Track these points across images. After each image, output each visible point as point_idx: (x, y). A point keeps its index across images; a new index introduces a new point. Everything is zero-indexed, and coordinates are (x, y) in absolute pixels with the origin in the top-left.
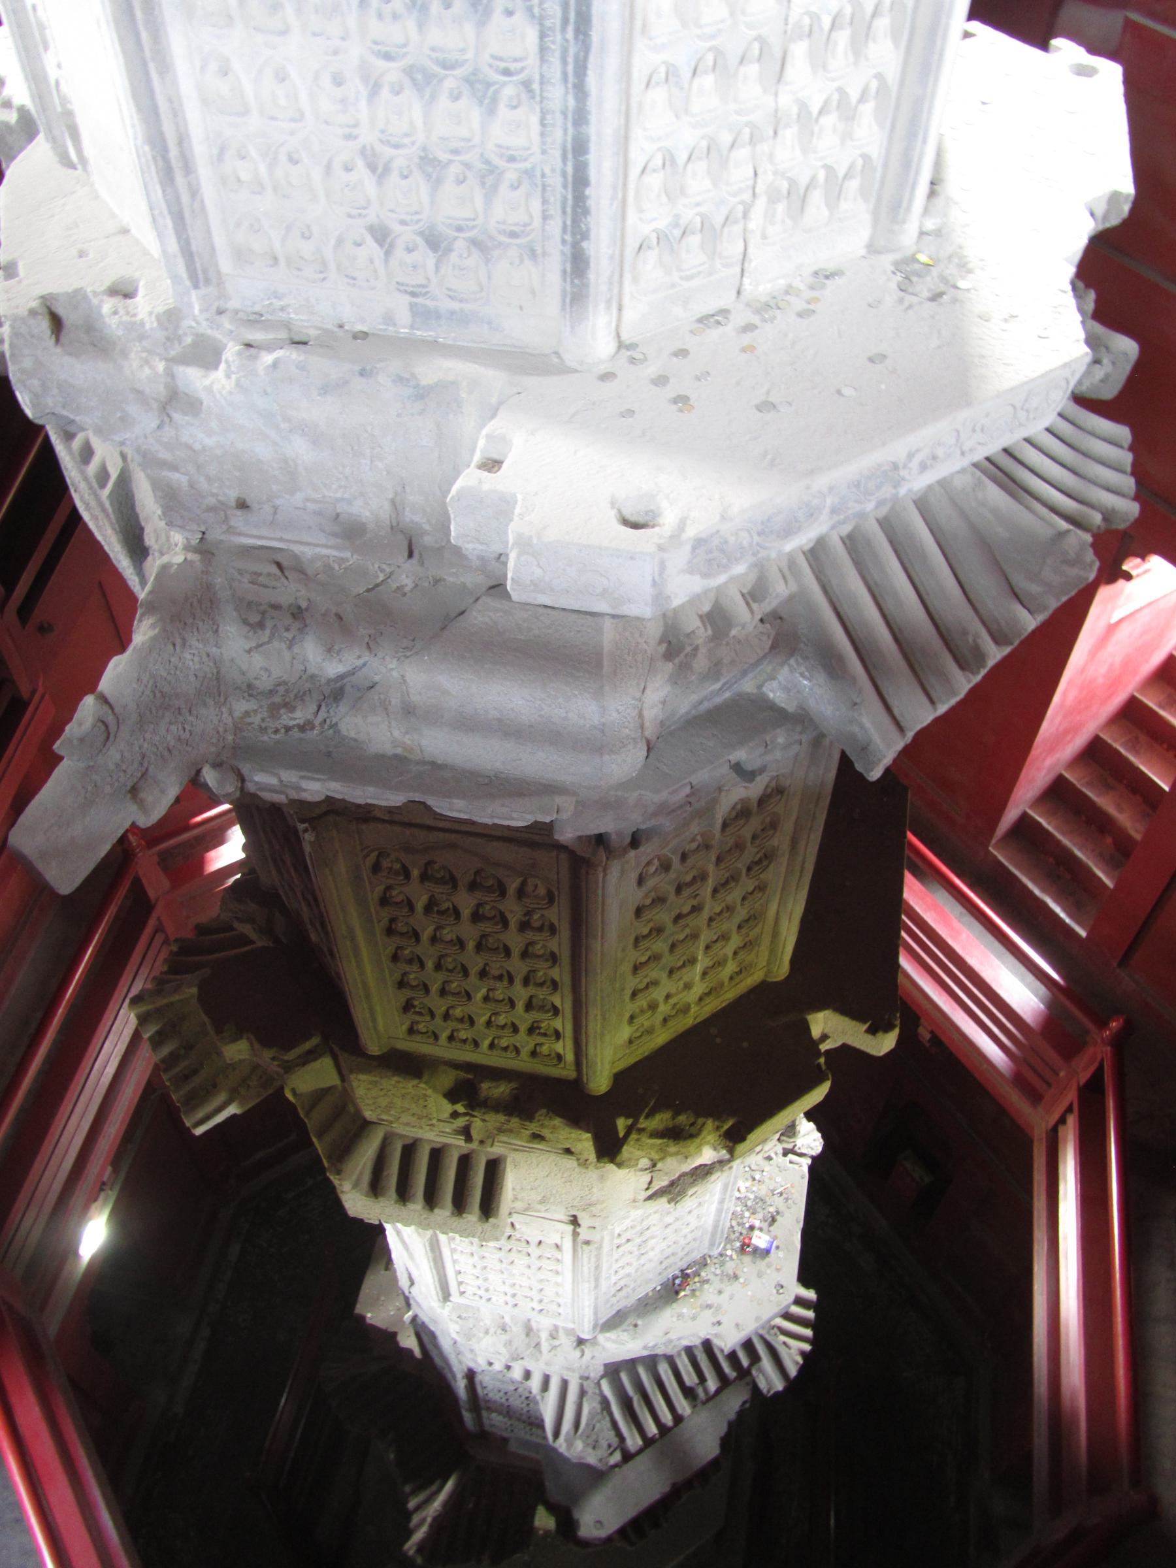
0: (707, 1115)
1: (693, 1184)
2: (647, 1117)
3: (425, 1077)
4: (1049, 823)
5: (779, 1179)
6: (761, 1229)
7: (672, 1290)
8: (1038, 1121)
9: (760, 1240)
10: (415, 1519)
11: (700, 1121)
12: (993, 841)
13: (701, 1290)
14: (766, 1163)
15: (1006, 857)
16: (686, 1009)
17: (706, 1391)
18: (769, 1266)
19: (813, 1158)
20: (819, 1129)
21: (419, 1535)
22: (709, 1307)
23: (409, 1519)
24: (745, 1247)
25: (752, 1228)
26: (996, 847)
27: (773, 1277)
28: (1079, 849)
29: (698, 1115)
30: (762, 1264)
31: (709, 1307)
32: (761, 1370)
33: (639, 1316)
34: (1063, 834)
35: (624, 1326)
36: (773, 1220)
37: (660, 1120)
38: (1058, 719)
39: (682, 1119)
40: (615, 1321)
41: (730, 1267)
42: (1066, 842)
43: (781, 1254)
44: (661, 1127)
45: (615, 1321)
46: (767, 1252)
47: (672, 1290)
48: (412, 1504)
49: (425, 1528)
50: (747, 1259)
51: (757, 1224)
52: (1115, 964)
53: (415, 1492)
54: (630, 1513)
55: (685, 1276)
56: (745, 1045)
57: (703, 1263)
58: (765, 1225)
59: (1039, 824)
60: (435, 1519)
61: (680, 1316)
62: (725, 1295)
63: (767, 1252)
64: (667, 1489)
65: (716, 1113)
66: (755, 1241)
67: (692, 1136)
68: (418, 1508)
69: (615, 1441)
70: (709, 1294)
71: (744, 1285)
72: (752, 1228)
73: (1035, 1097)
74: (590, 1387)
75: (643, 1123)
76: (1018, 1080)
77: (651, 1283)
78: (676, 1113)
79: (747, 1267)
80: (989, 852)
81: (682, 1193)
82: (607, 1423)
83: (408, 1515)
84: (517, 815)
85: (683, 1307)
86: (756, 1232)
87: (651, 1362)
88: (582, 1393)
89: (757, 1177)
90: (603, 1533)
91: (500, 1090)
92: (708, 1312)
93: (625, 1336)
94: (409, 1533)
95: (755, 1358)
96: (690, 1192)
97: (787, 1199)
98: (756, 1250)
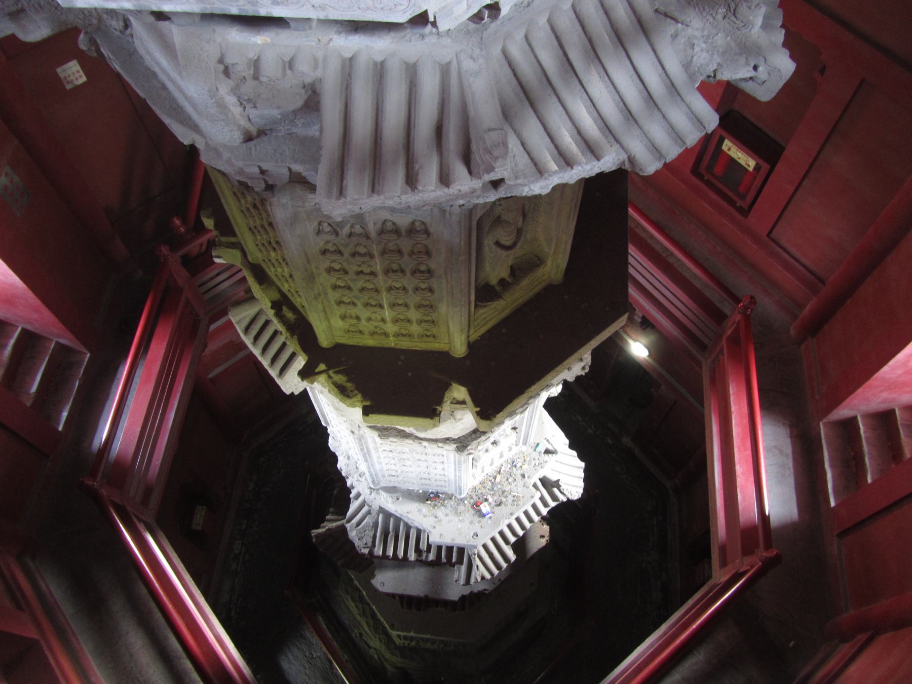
0: (360, 391)
1: (395, 436)
2: (335, 372)
3: (263, 287)
4: (865, 432)
5: (519, 489)
6: (490, 504)
7: (429, 497)
8: (719, 576)
9: (485, 508)
10: (326, 523)
11: (356, 392)
12: (825, 420)
13: (439, 507)
14: (520, 477)
15: (825, 435)
16: (386, 335)
17: (427, 557)
18: (479, 522)
19: (568, 499)
20: (585, 489)
21: (320, 531)
22: (436, 517)
23: (323, 522)
24: (476, 505)
25: (486, 500)
26: (824, 424)
27: (476, 528)
28: (870, 459)
29: (357, 388)
30: (476, 519)
31: (436, 517)
32: (459, 569)
33: (402, 496)
34: (868, 442)
35: (393, 495)
36: (499, 505)
37: (340, 378)
38: (899, 372)
39: (349, 385)
40: (391, 490)
41: (461, 508)
42: (865, 448)
43: (489, 522)
44: (339, 382)
45: (391, 490)
46: (484, 516)
47: (429, 497)
48: (328, 517)
49: (324, 530)
50: (472, 511)
51: (491, 500)
52: (835, 533)
53: (333, 513)
54: (399, 591)
55: (437, 495)
56: (410, 374)
57: (450, 497)
58: (493, 504)
59: (859, 428)
60: (329, 529)
61: (419, 511)
62: (448, 518)
63: (484, 516)
64: (422, 595)
65: (365, 396)
66: (482, 506)
67: (348, 397)
68: (330, 521)
69: (370, 544)
70: (440, 512)
71: (460, 521)
72: (486, 500)
73: (724, 563)
74: (374, 513)
75: (331, 372)
76: (723, 549)
77: (417, 488)
78: (348, 381)
79: (469, 515)
80: (818, 425)
81: (387, 436)
82: (372, 534)
83: (324, 520)
84: (185, 136)
85: (425, 508)
86: (486, 503)
87: (398, 520)
88: (369, 512)
89: (510, 480)
90: (381, 589)
91: (290, 315)
92: (433, 519)
93: (390, 500)
94: (319, 527)
95: (460, 562)
96: (391, 439)
97: (514, 501)
98: (480, 511)
